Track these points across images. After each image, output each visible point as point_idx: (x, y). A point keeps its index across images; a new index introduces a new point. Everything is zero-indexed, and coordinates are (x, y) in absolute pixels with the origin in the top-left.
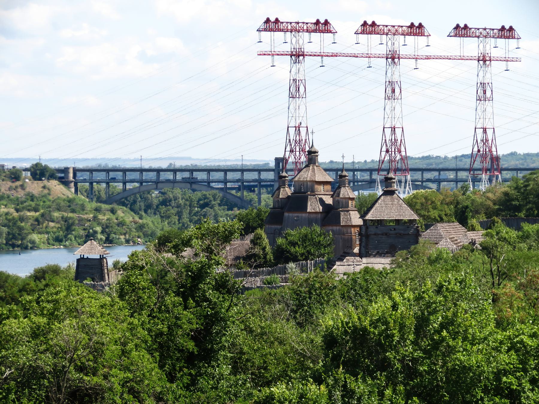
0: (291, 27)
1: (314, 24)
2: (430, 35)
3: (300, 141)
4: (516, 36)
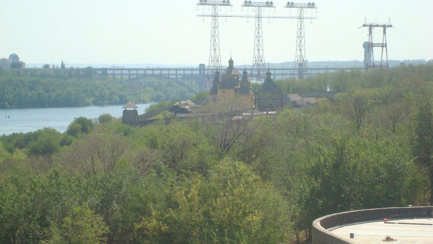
0: (212, 3)
2: (317, 8)
3: (216, 56)
4: (316, 7)
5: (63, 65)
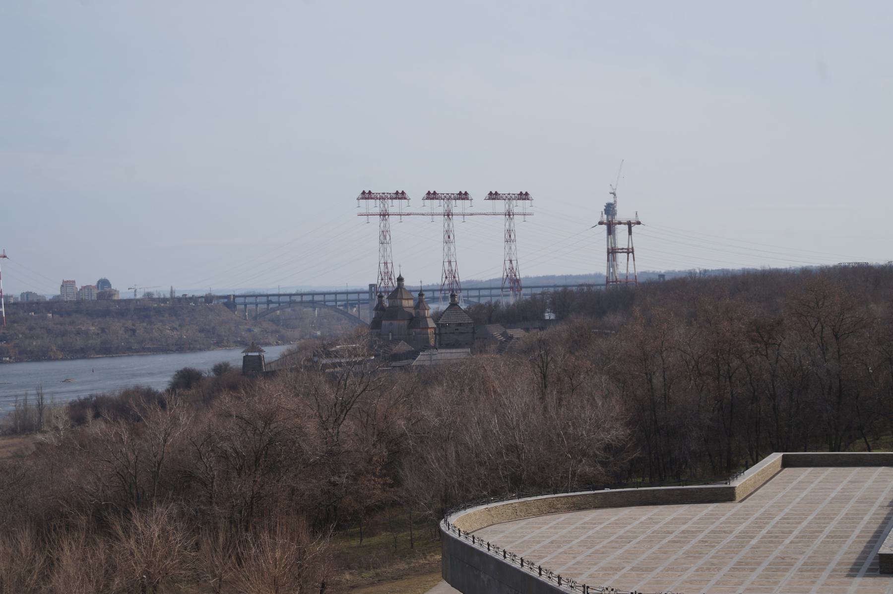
1: (395, 194)
5: (172, 292)
